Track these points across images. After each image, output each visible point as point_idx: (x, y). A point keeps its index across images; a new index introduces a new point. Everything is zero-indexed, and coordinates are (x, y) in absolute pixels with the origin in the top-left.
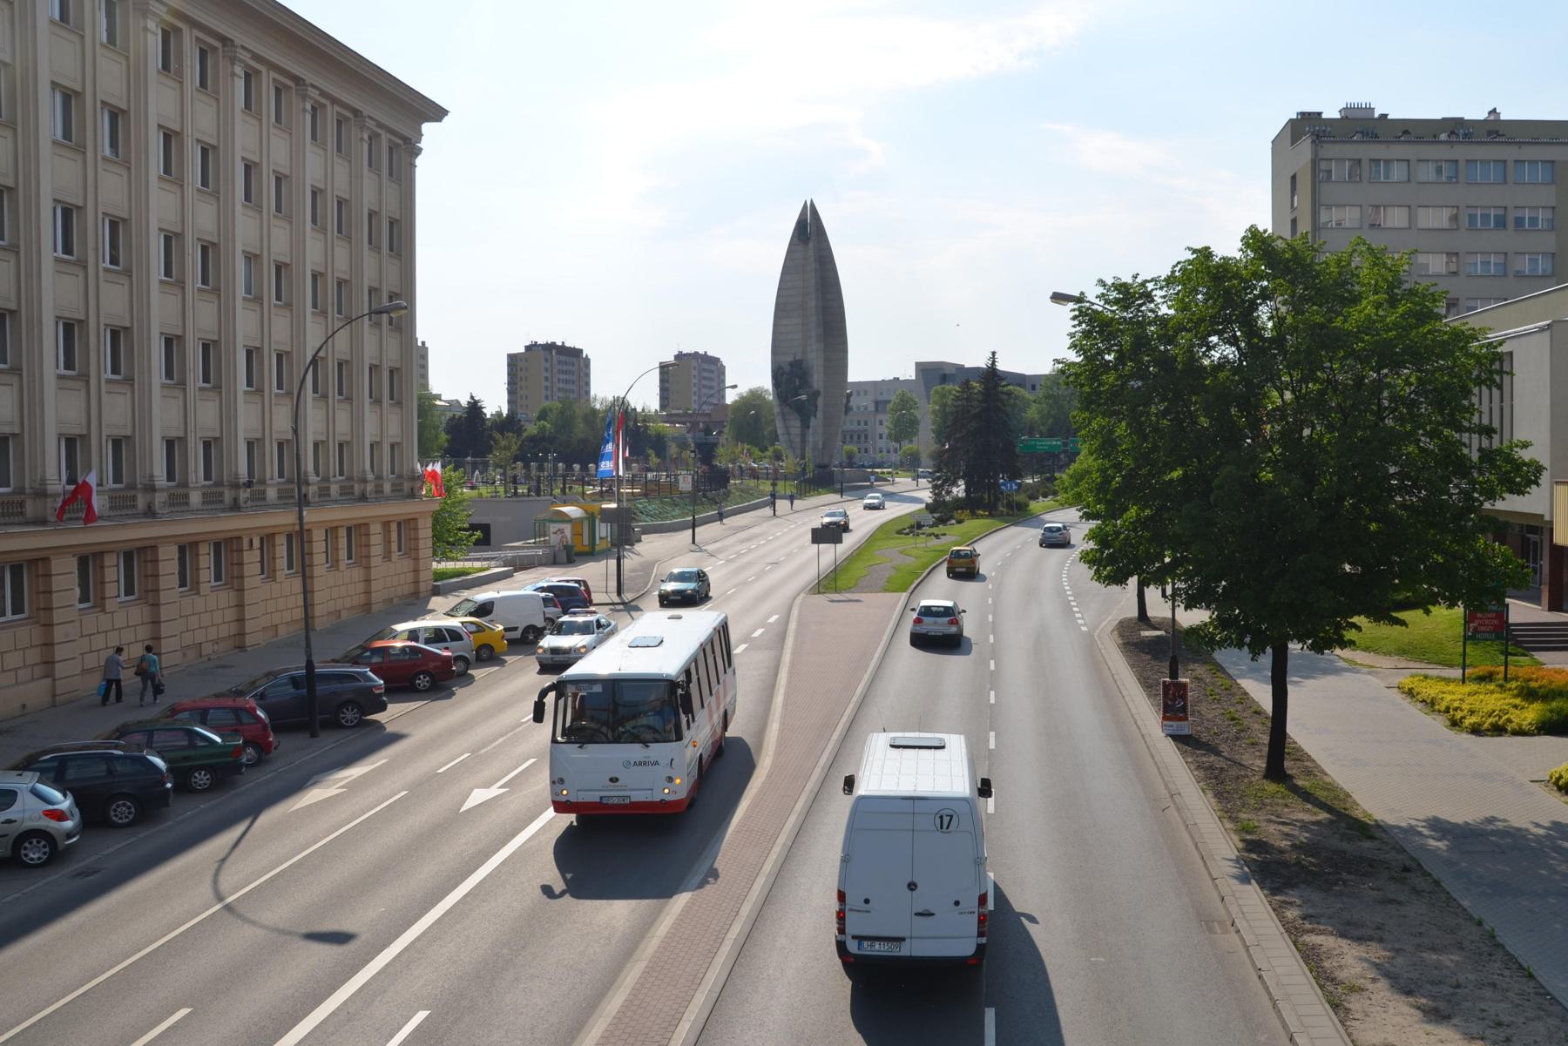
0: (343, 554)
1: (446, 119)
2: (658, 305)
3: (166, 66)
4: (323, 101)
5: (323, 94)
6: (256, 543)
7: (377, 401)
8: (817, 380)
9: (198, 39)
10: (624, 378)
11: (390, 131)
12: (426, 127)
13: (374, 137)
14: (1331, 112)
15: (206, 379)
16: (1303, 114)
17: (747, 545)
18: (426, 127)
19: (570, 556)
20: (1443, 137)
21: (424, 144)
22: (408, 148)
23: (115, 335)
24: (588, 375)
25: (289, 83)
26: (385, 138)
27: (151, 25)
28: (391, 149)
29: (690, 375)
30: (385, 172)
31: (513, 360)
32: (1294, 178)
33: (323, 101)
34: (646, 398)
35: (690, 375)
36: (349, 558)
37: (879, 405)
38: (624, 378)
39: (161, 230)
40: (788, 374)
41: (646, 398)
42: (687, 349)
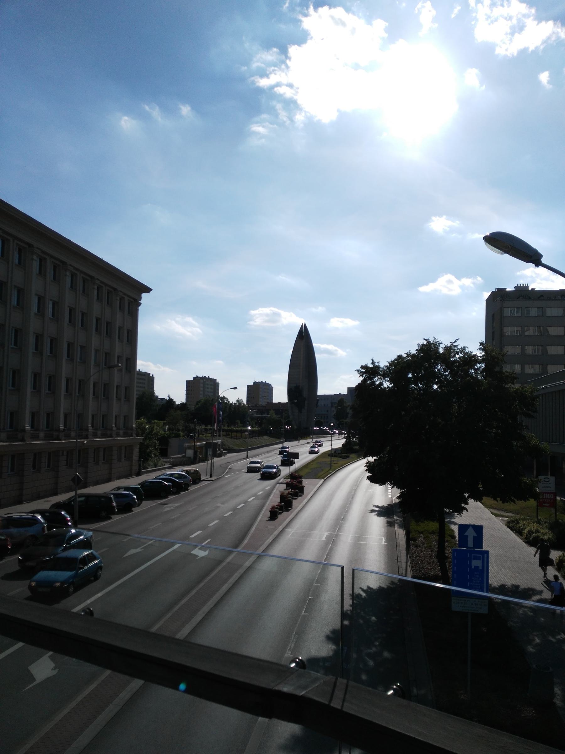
0: (101, 458)
1: (151, 292)
2: (247, 369)
3: (72, 287)
4: (102, 285)
5: (102, 282)
6: (65, 453)
7: (119, 399)
8: (305, 394)
9: (17, 244)
10: (234, 392)
11: (128, 296)
12: (143, 295)
13: (122, 299)
14: (510, 288)
15: (49, 390)
16: (498, 289)
17: (268, 459)
18: (143, 295)
19: (193, 461)
20: (559, 297)
21: (142, 301)
22: (137, 303)
23: (14, 372)
24: (272, 393)
25: (132, 300)
26: (126, 298)
27: (35, 257)
28: (129, 303)
29: (259, 390)
30: (126, 312)
31: (188, 382)
32: (493, 315)
33: (102, 285)
34: (180, 398)
35: (259, 390)
36: (104, 459)
37: (332, 404)
38: (234, 392)
39: (34, 333)
40: (293, 390)
41: (180, 398)
42: (258, 380)
